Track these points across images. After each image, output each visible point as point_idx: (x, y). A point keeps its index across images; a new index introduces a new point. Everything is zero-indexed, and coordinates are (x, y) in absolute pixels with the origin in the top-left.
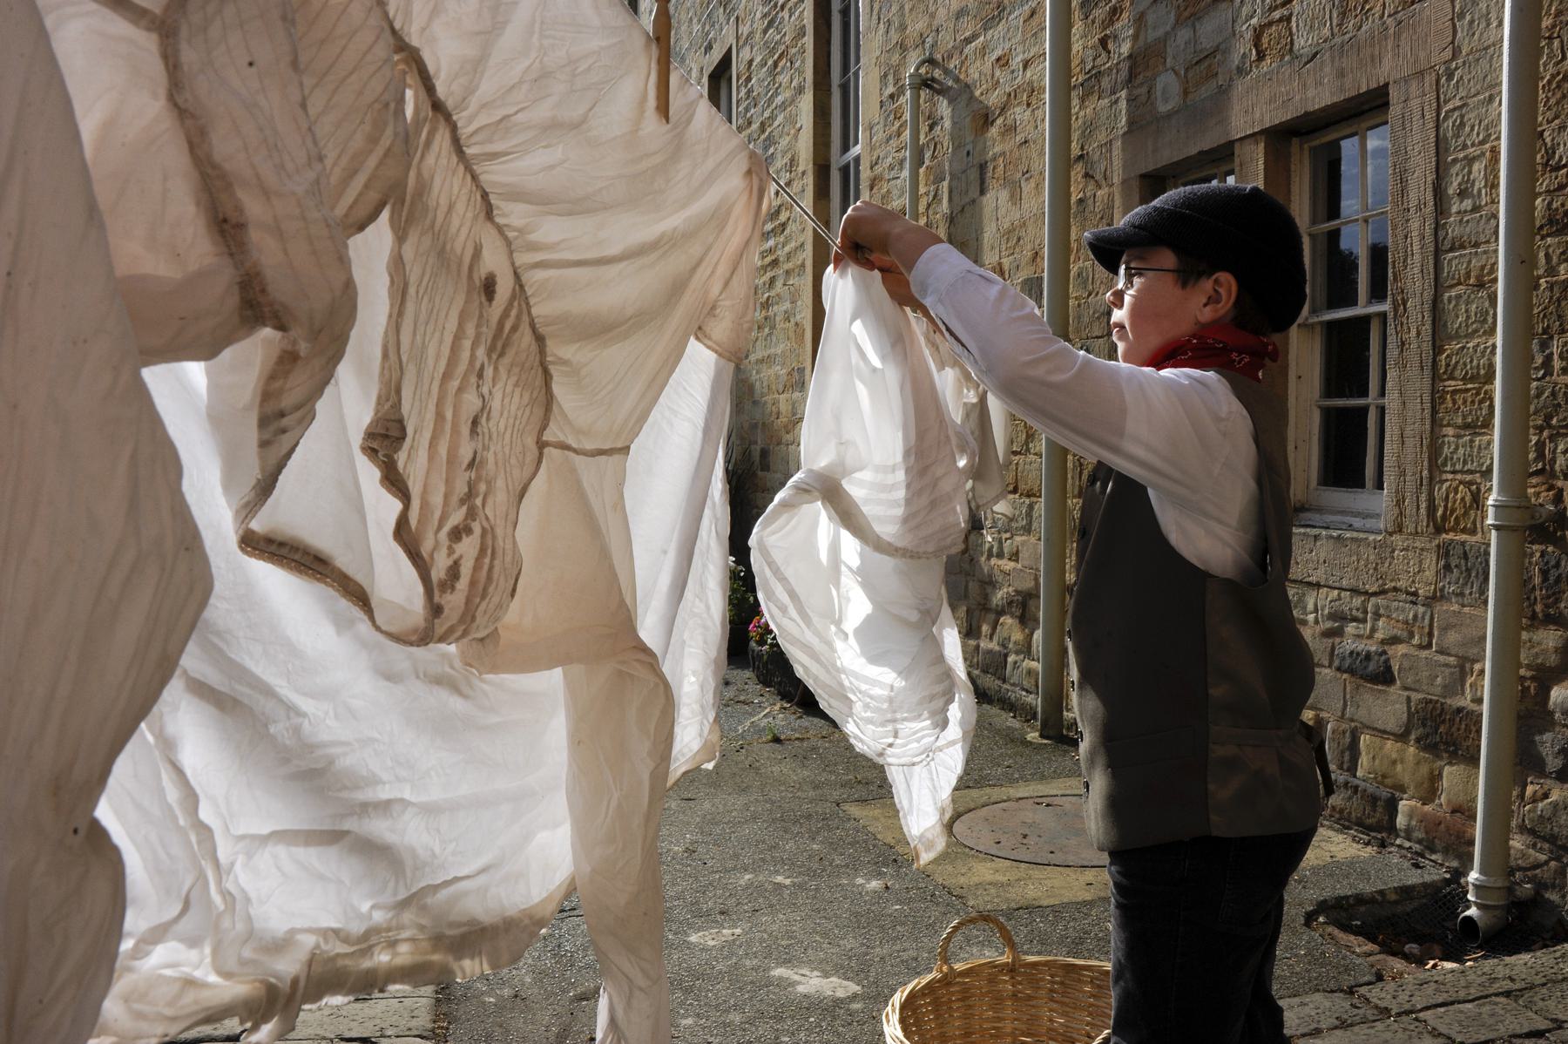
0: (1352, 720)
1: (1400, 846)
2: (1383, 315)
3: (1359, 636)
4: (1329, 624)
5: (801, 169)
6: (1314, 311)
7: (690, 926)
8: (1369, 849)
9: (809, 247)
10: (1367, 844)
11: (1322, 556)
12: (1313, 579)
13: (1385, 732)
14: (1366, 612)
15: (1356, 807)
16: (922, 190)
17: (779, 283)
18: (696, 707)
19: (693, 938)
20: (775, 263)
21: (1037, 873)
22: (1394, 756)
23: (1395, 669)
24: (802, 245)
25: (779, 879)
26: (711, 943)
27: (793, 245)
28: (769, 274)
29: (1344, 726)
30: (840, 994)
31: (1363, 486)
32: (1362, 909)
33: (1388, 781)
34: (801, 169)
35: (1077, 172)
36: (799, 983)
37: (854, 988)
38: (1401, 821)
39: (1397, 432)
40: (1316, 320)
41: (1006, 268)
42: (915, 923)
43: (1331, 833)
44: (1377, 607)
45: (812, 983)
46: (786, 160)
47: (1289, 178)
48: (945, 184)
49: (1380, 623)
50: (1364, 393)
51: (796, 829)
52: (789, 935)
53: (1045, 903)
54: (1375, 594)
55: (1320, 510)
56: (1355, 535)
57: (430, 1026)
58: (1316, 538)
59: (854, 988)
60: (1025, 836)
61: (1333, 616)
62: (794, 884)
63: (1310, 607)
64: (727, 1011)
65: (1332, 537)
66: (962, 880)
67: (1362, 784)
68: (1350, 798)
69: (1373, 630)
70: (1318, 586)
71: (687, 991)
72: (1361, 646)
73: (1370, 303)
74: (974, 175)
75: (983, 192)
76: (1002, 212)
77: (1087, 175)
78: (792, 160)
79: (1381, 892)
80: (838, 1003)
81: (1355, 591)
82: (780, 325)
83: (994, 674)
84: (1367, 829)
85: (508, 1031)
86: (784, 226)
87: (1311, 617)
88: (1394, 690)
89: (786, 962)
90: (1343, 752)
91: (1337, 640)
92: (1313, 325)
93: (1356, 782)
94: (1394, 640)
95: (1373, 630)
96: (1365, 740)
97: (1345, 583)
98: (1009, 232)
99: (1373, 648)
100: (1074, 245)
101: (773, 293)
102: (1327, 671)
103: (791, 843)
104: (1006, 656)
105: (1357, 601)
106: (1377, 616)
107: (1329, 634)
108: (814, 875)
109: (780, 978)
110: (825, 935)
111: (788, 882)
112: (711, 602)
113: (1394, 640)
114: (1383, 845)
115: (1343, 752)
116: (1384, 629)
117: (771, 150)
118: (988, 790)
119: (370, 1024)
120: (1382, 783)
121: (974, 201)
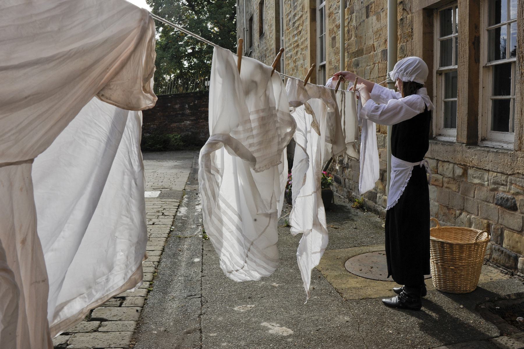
0: (501, 225)
1: (519, 275)
2: (515, 62)
3: (504, 192)
4: (493, 186)
5: (306, 10)
6: (489, 61)
7: (236, 303)
8: (507, 276)
9: (309, 40)
10: (506, 274)
11: (491, 159)
12: (487, 168)
13: (514, 230)
14: (507, 182)
15: (502, 259)
16: (346, 17)
17: (299, 54)
18: (123, 266)
19: (236, 309)
20: (298, 46)
21: (373, 284)
22: (517, 240)
23: (518, 205)
24: (306, 39)
25: (274, 284)
26: (242, 311)
27: (303, 39)
28: (296, 50)
29: (499, 227)
30: (285, 334)
31: (508, 131)
32: (501, 302)
33: (515, 250)
34: (306, 10)
35: (400, 8)
36: (271, 329)
37: (291, 332)
38: (519, 265)
39: (520, 110)
40: (490, 64)
41: (375, 46)
42: (321, 304)
43: (492, 269)
44: (511, 180)
45: (276, 329)
46: (301, 7)
47: (479, 9)
48: (354, 14)
49: (512, 187)
50: (509, 94)
51: (285, 263)
52: (272, 308)
53: (373, 297)
54: (510, 175)
55: (491, 140)
56: (503, 151)
57: (128, 343)
58: (488, 152)
59: (291, 332)
60: (372, 268)
61: (495, 183)
62: (279, 286)
63: (486, 179)
64: (240, 340)
65: (494, 152)
66: (343, 286)
67: (505, 250)
68: (500, 255)
69: (510, 189)
70: (489, 171)
71: (228, 331)
72: (505, 195)
73: (511, 57)
74: (364, 10)
75: (367, 17)
76: (374, 24)
77: (404, 9)
78: (303, 7)
79: (509, 295)
80: (283, 338)
81: (502, 173)
82: (300, 69)
83: (372, 201)
84: (507, 268)
85: (158, 345)
86: (300, 32)
87: (486, 183)
88: (517, 213)
89: (268, 320)
90: (498, 237)
91: (496, 193)
92: (489, 66)
93: (502, 249)
94: (518, 194)
95: (510, 189)
96: (506, 232)
97: (499, 170)
98: (377, 32)
99: (510, 197)
100: (399, 37)
101: (297, 57)
102: (492, 205)
103: (282, 269)
104: (376, 194)
105: (504, 177)
106: (511, 184)
107: (493, 190)
108: (287, 282)
109: (264, 327)
110: (285, 308)
111: (277, 285)
112: (134, 217)
113: (518, 194)
114: (512, 275)
115: (498, 237)
116: (514, 189)
117: (296, 4)
118: (362, 248)
119: (106, 343)
120: (512, 250)
121: (364, 21)
